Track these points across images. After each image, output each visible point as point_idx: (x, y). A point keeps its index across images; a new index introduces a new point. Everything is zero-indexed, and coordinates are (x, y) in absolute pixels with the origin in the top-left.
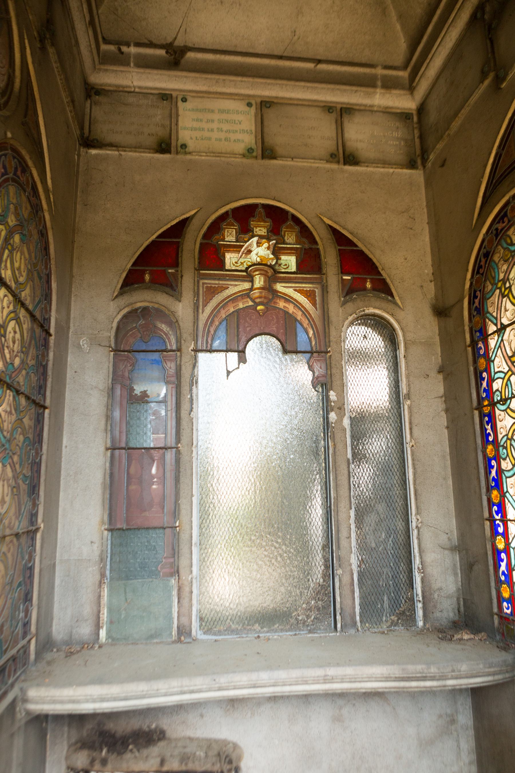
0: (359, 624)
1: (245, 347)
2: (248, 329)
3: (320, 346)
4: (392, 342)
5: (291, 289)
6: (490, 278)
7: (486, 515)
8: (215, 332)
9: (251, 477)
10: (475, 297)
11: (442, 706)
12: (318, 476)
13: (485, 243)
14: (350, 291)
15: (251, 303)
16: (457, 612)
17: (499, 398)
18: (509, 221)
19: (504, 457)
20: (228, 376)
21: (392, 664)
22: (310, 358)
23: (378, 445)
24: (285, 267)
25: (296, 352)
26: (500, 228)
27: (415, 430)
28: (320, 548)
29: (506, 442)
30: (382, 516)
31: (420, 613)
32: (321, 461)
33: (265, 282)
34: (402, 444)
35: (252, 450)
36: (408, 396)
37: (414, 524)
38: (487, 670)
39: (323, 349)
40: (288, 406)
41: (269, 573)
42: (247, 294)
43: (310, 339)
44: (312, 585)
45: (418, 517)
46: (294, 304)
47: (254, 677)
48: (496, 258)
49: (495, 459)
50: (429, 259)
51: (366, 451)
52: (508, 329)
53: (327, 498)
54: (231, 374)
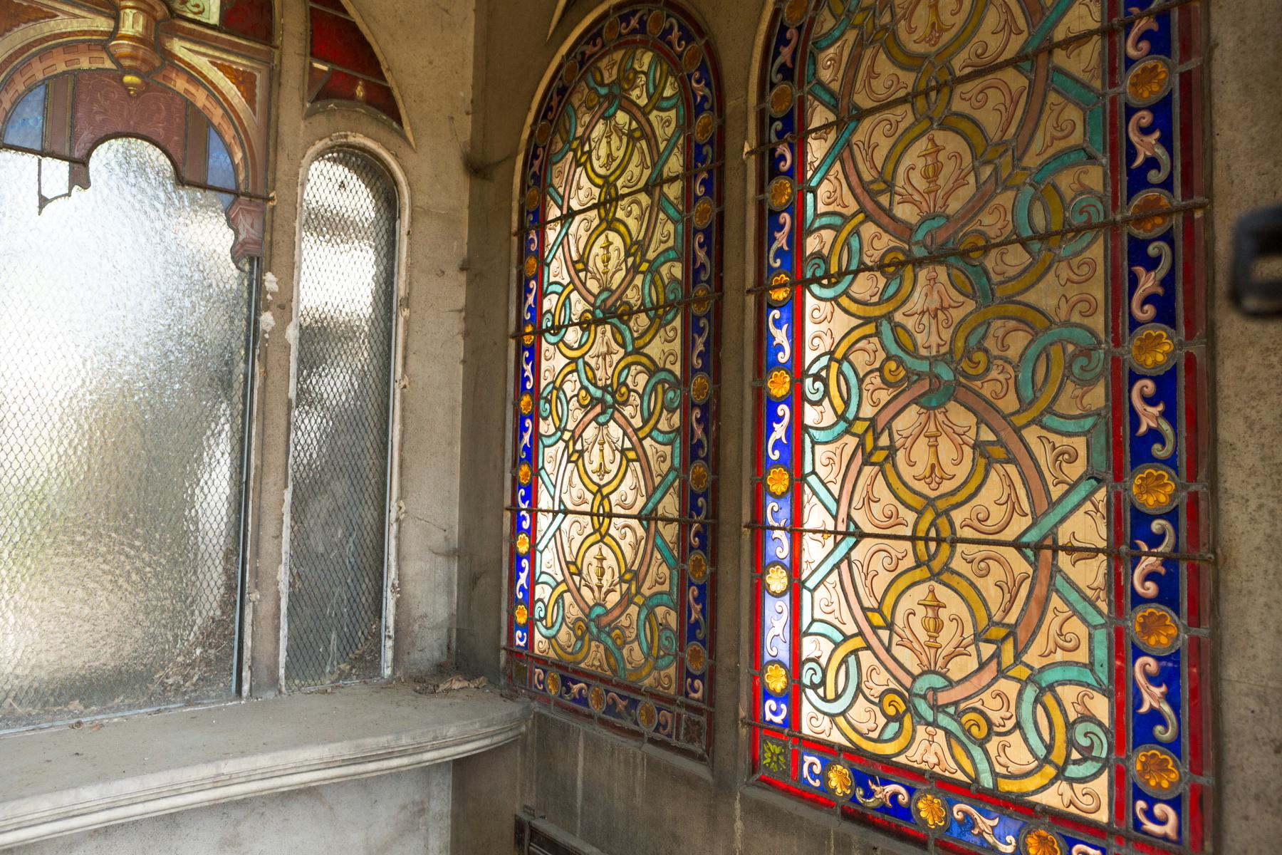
0: (283, 682)
1: (89, 155)
2: (99, 118)
3: (255, 183)
4: (389, 205)
5: (205, 60)
6: (562, 130)
7: (508, 502)
8: (15, 104)
9: (82, 421)
10: (535, 156)
11: (408, 793)
12: (227, 427)
13: (563, 72)
14: (325, 93)
15: (108, 64)
16: (445, 649)
17: (549, 324)
18: (603, 46)
19: (545, 414)
20: (41, 207)
21: (340, 740)
22: (233, 203)
23: (336, 383)
24: (196, 10)
25: (205, 187)
26: (588, 53)
27: (412, 360)
28: (221, 555)
29: (551, 392)
30: (340, 501)
31: (388, 655)
32: (235, 399)
33: (146, 27)
34: (388, 384)
35: (89, 366)
36: (406, 302)
37: (393, 516)
38: (484, 731)
39: (259, 192)
40: (177, 289)
41: (110, 604)
42: (103, 42)
43: (235, 167)
44: (199, 621)
45: (402, 503)
46: (208, 90)
47: (66, 799)
48: (576, 100)
49: (531, 418)
50: (469, 73)
51: (323, 389)
52: (578, 219)
53: (241, 466)
54: (49, 207)
